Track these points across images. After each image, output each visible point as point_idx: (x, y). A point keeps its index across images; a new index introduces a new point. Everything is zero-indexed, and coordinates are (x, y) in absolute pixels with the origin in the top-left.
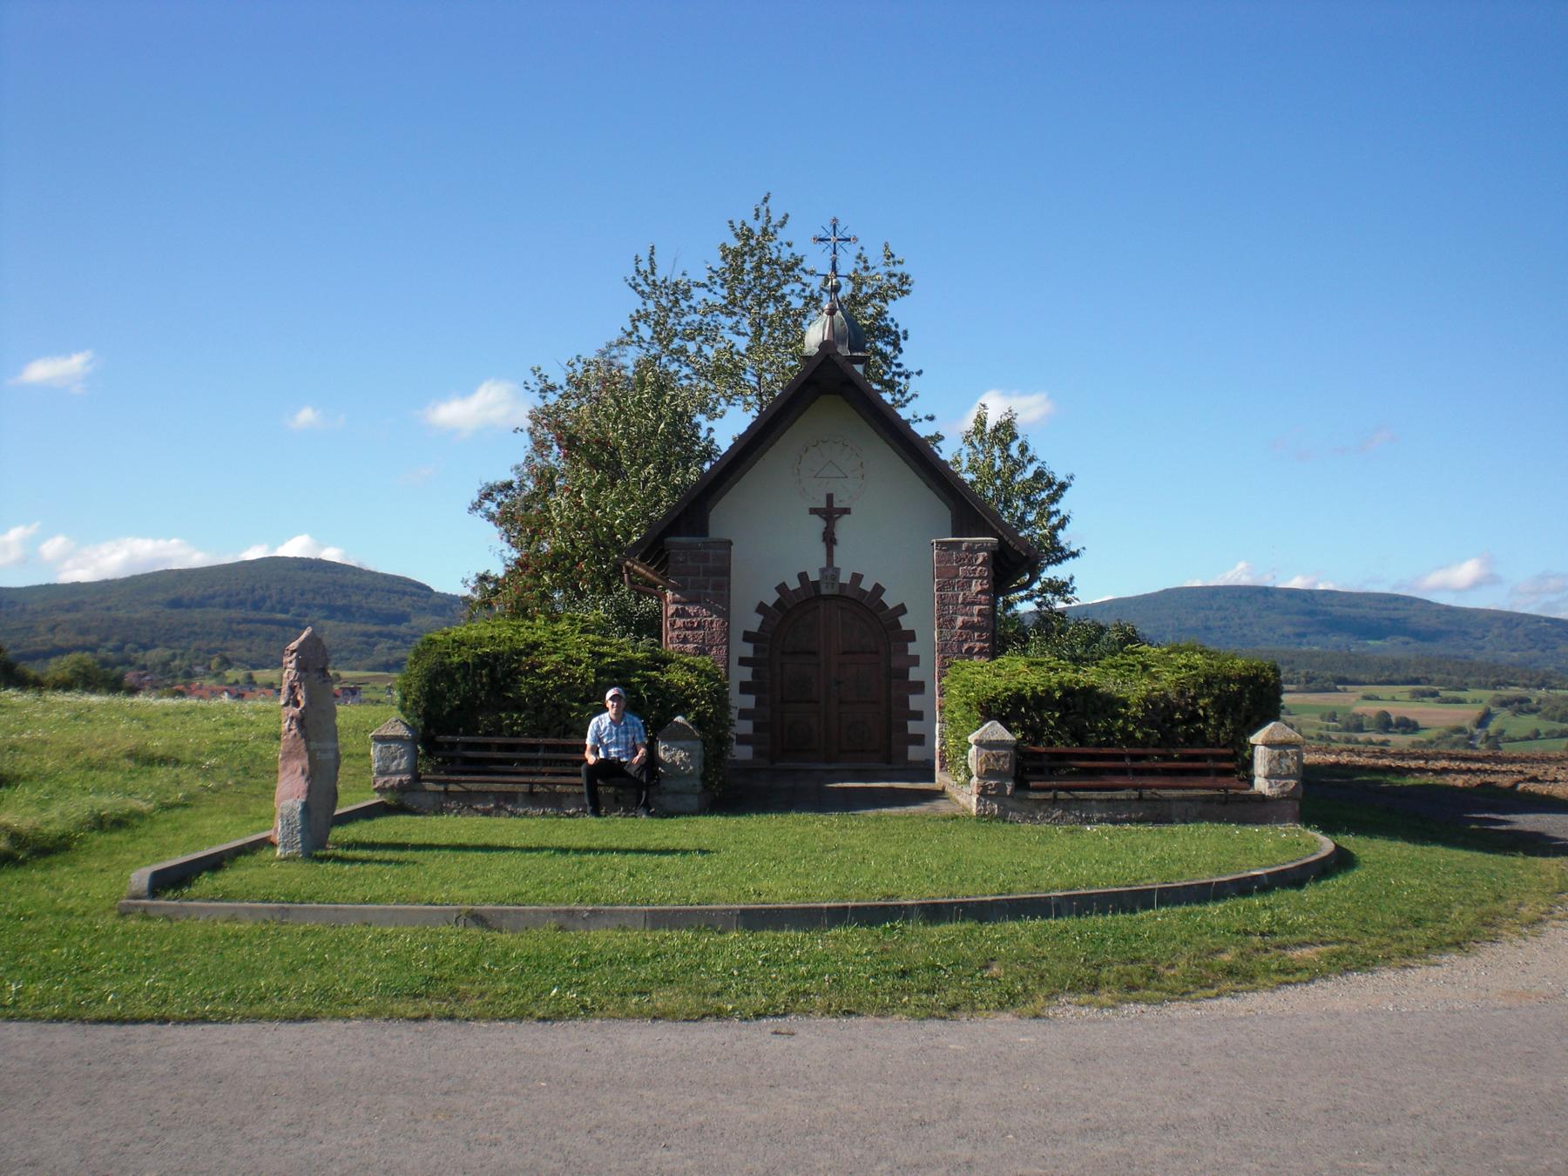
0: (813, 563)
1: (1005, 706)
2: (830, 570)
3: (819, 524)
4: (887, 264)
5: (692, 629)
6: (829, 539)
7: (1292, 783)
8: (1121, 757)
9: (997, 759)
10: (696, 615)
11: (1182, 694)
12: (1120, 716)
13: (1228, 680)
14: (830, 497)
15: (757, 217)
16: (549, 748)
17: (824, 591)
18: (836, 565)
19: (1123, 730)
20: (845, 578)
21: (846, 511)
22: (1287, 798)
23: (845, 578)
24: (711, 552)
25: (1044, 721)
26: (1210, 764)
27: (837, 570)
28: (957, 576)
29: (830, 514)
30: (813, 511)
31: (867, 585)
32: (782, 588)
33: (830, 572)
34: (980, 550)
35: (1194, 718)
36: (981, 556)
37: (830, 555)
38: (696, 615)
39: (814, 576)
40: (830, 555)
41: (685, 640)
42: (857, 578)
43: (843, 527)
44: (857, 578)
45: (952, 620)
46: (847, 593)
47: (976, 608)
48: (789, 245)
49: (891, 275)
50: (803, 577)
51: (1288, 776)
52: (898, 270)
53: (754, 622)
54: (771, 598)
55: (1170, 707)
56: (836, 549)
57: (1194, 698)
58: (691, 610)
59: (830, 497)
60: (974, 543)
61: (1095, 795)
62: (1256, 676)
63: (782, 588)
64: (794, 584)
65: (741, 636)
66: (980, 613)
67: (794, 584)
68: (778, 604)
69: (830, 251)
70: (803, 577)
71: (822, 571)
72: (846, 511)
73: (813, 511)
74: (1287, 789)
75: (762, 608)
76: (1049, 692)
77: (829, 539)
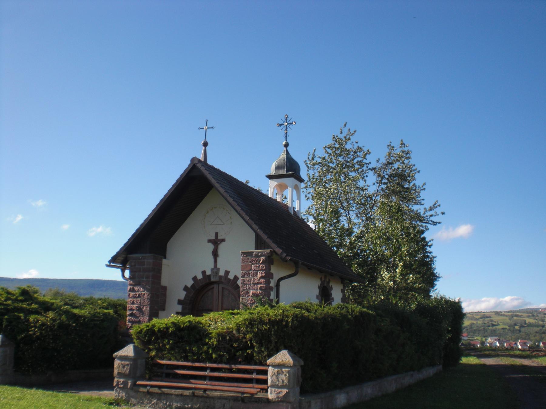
0: (208, 266)
1: (146, 336)
2: (215, 269)
3: (211, 247)
4: (401, 147)
5: (136, 297)
6: (215, 254)
7: (285, 391)
8: (204, 369)
9: (124, 367)
10: (138, 291)
11: (238, 330)
12: (207, 344)
13: (262, 322)
14: (217, 234)
15: (341, 133)
16: (213, 370)
17: (213, 279)
18: (218, 267)
19: (207, 352)
20: (222, 273)
21: (223, 240)
22: (281, 401)
23: (222, 273)
24: (146, 260)
25: (164, 345)
26: (254, 376)
27: (219, 269)
28: (251, 270)
29: (216, 242)
30: (210, 241)
31: (231, 277)
32: (195, 279)
33: (215, 270)
34: (261, 256)
35: (246, 347)
36: (262, 258)
37: (216, 262)
38: (138, 291)
39: (208, 273)
40: (216, 262)
41: (133, 303)
42: (227, 273)
43: (222, 248)
44: (227, 273)
45: (248, 293)
47: (259, 286)
48: (357, 143)
49: (403, 152)
50: (204, 272)
51: (283, 387)
52: (406, 149)
53: (182, 295)
54: (190, 283)
55: (233, 339)
56: (219, 259)
57: (245, 334)
58: (137, 288)
59: (217, 234)
60: (259, 252)
61: (173, 391)
62: (281, 320)
63: (195, 279)
64: (200, 277)
65: (176, 302)
66: (261, 288)
67: (200, 277)
68: (193, 286)
69: (284, 129)
70: (204, 272)
71: (212, 270)
72: (223, 240)
73: (210, 241)
74: (281, 395)
75: (186, 288)
76: (167, 328)
77: (215, 254)
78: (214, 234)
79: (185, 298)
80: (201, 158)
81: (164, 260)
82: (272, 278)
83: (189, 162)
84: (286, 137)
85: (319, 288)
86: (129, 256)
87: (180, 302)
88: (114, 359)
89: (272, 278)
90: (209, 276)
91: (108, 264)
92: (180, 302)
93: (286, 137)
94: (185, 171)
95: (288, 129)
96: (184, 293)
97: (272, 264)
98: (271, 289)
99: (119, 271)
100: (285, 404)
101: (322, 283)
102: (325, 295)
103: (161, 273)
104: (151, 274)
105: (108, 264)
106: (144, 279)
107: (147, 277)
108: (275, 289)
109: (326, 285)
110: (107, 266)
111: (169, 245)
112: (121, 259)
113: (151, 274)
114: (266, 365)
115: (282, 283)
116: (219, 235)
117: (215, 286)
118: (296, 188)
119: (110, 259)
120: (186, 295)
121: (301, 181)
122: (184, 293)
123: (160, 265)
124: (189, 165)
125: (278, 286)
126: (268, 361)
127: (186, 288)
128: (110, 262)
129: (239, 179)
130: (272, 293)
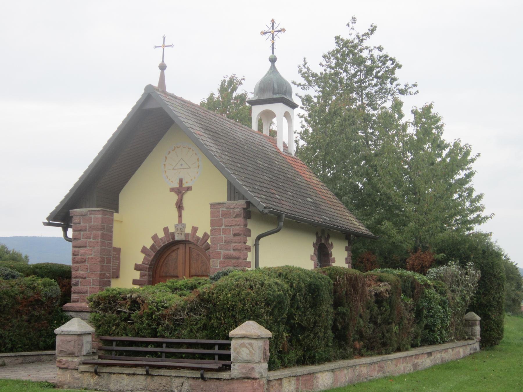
6: (180, 207)
14: (181, 181)
17: (177, 238)
20: (188, 230)
21: (189, 189)
24: (93, 216)
27: (184, 226)
29: (181, 191)
30: (172, 190)
32: (155, 237)
33: (180, 226)
37: (180, 216)
39: (172, 230)
40: (180, 216)
42: (195, 229)
43: (187, 198)
44: (195, 229)
46: (190, 239)
50: (166, 230)
53: (140, 258)
54: (149, 243)
56: (184, 213)
59: (181, 181)
63: (155, 237)
64: (161, 235)
67: (161, 235)
68: (153, 247)
70: (166, 230)
71: (176, 226)
72: (189, 189)
73: (172, 190)
75: (144, 250)
77: (180, 207)
78: (178, 181)
79: (143, 263)
80: (156, 84)
81: (115, 214)
82: (250, 236)
83: (143, 91)
84: (273, 48)
85: (314, 245)
86: (71, 211)
87: (137, 268)
88: (56, 335)
89: (250, 236)
90: (173, 234)
91: (47, 221)
92: (137, 268)
93: (273, 48)
94: (138, 102)
95: (276, 38)
96: (143, 256)
97: (250, 218)
98: (248, 249)
99: (60, 229)
100: (250, 381)
101: (319, 239)
102: (323, 254)
103: (112, 232)
104: (99, 232)
105: (47, 221)
106: (91, 240)
107: (95, 237)
108: (253, 249)
109: (323, 241)
110: (45, 224)
111: (121, 195)
112: (62, 217)
113: (99, 232)
114: (228, 338)
115: (262, 240)
116: (184, 182)
117: (181, 247)
118: (287, 115)
119: (48, 215)
120: (145, 258)
121: (293, 106)
122: (143, 256)
123: (112, 221)
124: (143, 95)
125: (256, 245)
126: (232, 333)
127: (144, 250)
128: (48, 219)
129: (29, 236)
130: (249, 254)
